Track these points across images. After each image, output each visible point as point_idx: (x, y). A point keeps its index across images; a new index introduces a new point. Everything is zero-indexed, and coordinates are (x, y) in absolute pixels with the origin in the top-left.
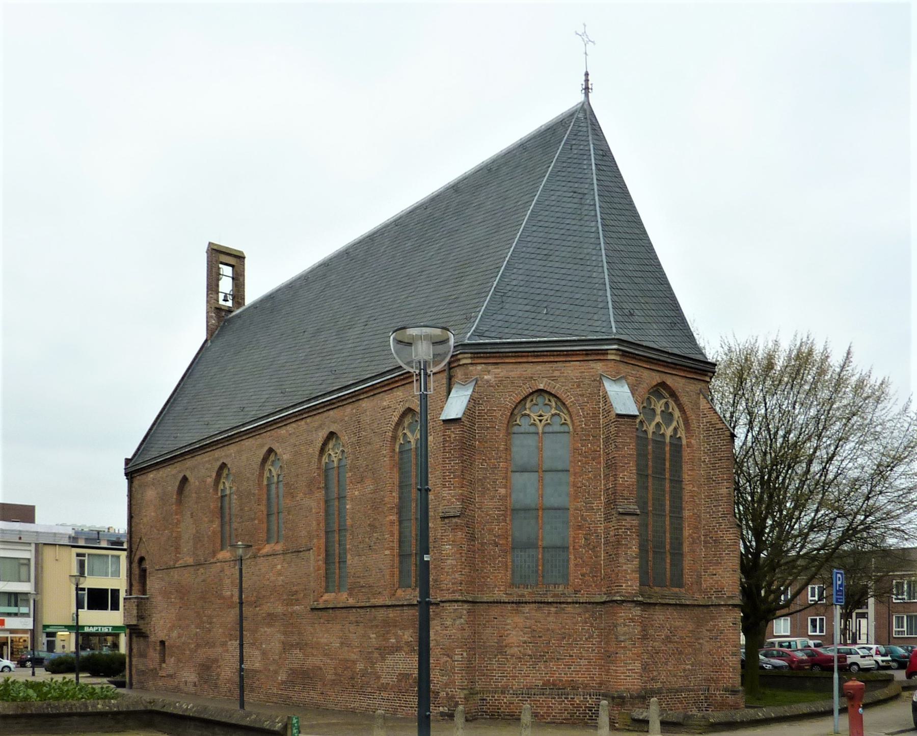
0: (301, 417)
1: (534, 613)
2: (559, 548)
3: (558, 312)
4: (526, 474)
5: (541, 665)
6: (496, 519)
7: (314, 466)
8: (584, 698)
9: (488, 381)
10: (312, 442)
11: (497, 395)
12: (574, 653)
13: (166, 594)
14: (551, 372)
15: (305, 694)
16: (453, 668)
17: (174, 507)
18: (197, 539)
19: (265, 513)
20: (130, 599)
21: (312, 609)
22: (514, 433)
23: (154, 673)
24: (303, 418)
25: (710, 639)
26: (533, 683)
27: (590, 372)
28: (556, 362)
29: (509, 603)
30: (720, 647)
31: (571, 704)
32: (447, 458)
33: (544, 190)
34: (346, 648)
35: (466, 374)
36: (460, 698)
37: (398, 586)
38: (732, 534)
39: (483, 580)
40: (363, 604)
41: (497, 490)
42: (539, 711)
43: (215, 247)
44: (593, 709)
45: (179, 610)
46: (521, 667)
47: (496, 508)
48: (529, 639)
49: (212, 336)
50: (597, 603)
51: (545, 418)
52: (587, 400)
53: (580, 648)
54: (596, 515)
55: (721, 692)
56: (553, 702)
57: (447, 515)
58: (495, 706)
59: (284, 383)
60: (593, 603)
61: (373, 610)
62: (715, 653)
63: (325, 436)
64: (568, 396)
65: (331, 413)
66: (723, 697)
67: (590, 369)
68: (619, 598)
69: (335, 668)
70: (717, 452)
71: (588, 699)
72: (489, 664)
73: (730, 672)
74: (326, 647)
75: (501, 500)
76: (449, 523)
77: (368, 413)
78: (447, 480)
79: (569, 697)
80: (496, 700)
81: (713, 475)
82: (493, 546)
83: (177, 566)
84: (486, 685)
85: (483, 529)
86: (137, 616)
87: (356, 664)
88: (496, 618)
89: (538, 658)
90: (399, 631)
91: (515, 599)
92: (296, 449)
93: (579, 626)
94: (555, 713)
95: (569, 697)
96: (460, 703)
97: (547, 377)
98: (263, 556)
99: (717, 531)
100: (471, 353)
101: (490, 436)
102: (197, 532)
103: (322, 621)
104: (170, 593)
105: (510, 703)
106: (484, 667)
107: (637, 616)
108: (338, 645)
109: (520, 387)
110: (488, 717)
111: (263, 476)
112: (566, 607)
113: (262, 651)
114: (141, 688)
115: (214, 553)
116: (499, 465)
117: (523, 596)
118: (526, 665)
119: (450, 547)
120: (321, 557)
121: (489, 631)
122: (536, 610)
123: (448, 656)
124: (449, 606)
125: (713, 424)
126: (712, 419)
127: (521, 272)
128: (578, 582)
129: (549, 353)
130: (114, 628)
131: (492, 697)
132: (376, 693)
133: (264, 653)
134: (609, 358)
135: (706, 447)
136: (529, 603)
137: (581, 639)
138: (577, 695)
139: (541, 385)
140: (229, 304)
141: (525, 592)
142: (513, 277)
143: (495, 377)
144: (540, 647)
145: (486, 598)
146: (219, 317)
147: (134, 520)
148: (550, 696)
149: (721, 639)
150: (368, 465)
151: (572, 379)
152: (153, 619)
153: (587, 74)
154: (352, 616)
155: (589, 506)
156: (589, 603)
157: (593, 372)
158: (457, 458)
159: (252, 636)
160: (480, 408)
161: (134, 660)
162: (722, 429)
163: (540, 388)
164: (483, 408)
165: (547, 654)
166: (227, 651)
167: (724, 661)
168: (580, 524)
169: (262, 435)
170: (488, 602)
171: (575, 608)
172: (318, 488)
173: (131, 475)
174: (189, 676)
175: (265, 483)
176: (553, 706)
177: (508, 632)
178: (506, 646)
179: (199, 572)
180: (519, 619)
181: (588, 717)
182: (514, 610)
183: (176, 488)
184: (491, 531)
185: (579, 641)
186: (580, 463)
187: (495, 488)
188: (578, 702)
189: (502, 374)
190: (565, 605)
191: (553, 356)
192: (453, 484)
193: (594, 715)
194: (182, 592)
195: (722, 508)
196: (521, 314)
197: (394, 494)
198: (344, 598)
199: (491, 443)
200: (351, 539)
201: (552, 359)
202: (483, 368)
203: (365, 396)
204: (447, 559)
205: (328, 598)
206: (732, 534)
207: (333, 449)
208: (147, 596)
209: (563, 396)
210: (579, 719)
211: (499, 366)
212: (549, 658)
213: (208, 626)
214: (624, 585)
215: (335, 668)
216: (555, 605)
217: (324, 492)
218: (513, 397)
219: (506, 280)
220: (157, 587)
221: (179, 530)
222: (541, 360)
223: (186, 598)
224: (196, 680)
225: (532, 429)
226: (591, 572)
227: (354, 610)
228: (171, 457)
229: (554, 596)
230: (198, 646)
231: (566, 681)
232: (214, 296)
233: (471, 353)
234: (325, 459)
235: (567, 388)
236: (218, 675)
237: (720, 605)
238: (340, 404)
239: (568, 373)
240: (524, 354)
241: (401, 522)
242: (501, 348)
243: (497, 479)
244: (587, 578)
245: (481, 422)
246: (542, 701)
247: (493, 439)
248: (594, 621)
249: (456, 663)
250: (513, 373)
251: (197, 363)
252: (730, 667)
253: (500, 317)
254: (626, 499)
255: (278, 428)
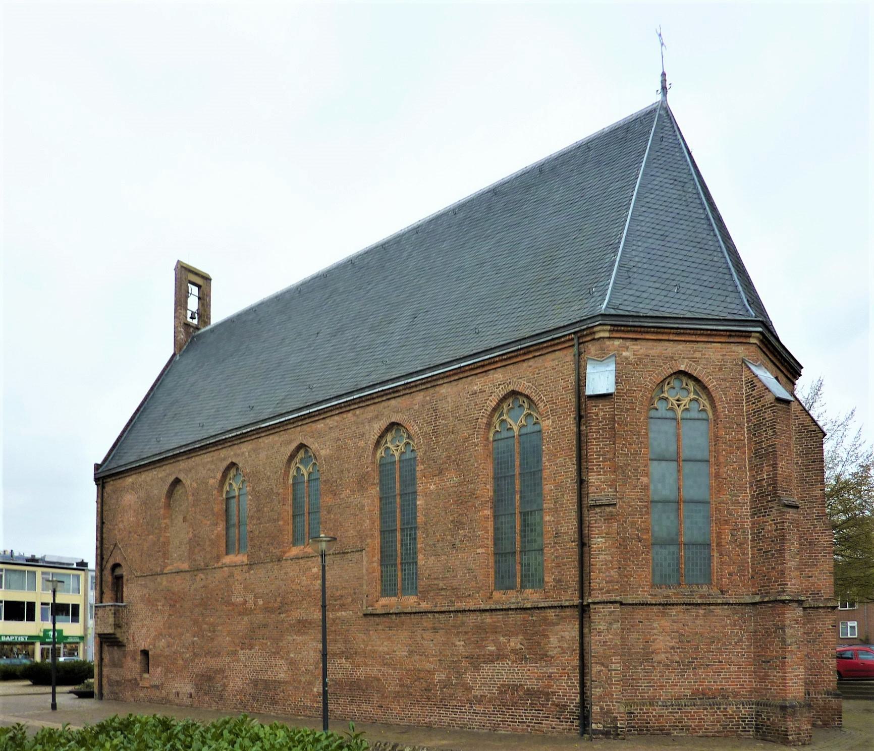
0: (348, 408)
1: (681, 616)
2: (700, 544)
3: (689, 292)
4: (664, 464)
5: (690, 672)
6: (639, 511)
7: (367, 459)
8: (736, 708)
9: (626, 358)
10: (363, 435)
11: (636, 374)
12: (724, 659)
13: (150, 602)
14: (692, 352)
15: (354, 707)
16: (610, 678)
17: (162, 511)
18: (195, 543)
19: (291, 513)
20: (100, 607)
21: (365, 615)
22: (652, 418)
23: (134, 684)
24: (351, 410)
25: (808, 642)
26: (681, 692)
27: (732, 355)
28: (697, 342)
29: (655, 605)
30: (819, 650)
31: (724, 715)
32: (594, 439)
33: (644, 174)
34: (418, 657)
35: (602, 349)
36: (619, 713)
37: (493, 588)
38: (827, 536)
39: (626, 580)
40: (443, 609)
41: (639, 479)
42: (690, 724)
43: (185, 266)
44: (747, 720)
45: (168, 618)
46: (668, 676)
47: (639, 499)
48: (677, 645)
49: (180, 349)
50: (747, 604)
51: (684, 402)
52: (730, 385)
53: (730, 652)
54: (742, 509)
55: (823, 696)
56: (705, 713)
57: (598, 503)
58: (643, 720)
59: (306, 380)
60: (742, 604)
61: (459, 615)
62: (813, 656)
63: (383, 428)
64: (710, 379)
65: (393, 402)
66: (825, 701)
67: (732, 352)
68: (787, 598)
69: (400, 680)
70: (810, 454)
71: (741, 709)
72: (634, 672)
73: (830, 675)
74: (388, 656)
75: (642, 489)
76: (601, 512)
77: (449, 399)
78: (595, 463)
79: (722, 707)
80: (644, 713)
81: (806, 477)
82: (637, 541)
83: (165, 572)
84: (632, 696)
85: (625, 522)
86: (114, 625)
87: (434, 674)
88: (642, 622)
89: (688, 665)
90: (502, 638)
91: (662, 601)
92: (340, 443)
93: (728, 629)
94: (707, 725)
95: (722, 707)
96: (619, 718)
97: (688, 358)
98: (291, 559)
99: (812, 533)
100: (611, 325)
101: (630, 419)
102: (195, 536)
103: (380, 627)
104: (157, 600)
105: (659, 716)
106: (630, 676)
107: (800, 617)
108: (405, 653)
109: (661, 366)
110: (636, 732)
111: (289, 474)
112: (713, 609)
113: (288, 661)
114: (115, 699)
115: (218, 558)
116: (641, 451)
117: (668, 597)
118: (675, 672)
119: (603, 540)
120: (375, 559)
121: (634, 635)
122: (684, 613)
123: (603, 664)
124: (603, 608)
125: (805, 426)
126: (804, 421)
127: (640, 249)
128: (726, 582)
129: (692, 331)
130: (30, 637)
131: (640, 710)
132: (465, 706)
133: (292, 663)
134: (751, 342)
135: (799, 449)
136: (677, 604)
137: (730, 643)
138: (730, 705)
139: (682, 366)
140: (195, 322)
141: (670, 592)
142: (634, 253)
143: (634, 355)
144: (688, 652)
145: (630, 600)
146: (187, 333)
147: (107, 526)
148: (702, 707)
149: (819, 642)
150: (449, 456)
151: (713, 362)
152: (132, 627)
153: (664, 75)
154: (428, 621)
155: (736, 500)
156: (739, 604)
157: (735, 355)
158: (608, 438)
159: (275, 646)
160: (619, 387)
161: (106, 671)
162: (815, 431)
163: (680, 369)
164: (622, 388)
165: (695, 661)
166: (238, 660)
167: (823, 663)
168: (726, 518)
169: (289, 431)
170: (633, 604)
171: (723, 609)
172: (373, 484)
173: (103, 480)
174: (184, 687)
175: (291, 481)
176: (705, 718)
177: (655, 637)
178: (653, 653)
179: (198, 578)
180: (665, 623)
181: (741, 729)
182: (659, 612)
183: (165, 491)
184: (633, 524)
185: (728, 645)
186: (724, 452)
187: (637, 476)
188: (731, 712)
189: (641, 351)
190: (713, 607)
191: (696, 335)
192: (603, 468)
193: (747, 727)
194: (174, 600)
195: (816, 510)
196: (651, 290)
197: (488, 487)
198: (411, 602)
199: (632, 427)
200: (424, 538)
201: (693, 338)
202: (621, 343)
203: (446, 380)
204: (598, 554)
205: (385, 603)
206: (827, 536)
207: (392, 442)
208: (124, 604)
209: (705, 380)
210: (733, 731)
211: (639, 342)
212: (698, 665)
213: (209, 634)
214: (789, 583)
215: (400, 680)
216: (703, 607)
217: (378, 489)
218: (654, 377)
219: (627, 256)
220: (137, 594)
221: (168, 535)
222: (683, 339)
223: (178, 605)
224: (193, 691)
225: (670, 414)
226: (738, 571)
227: (430, 615)
228: (159, 460)
229: (701, 597)
230: (195, 655)
231: (716, 689)
232: (183, 312)
233: (611, 325)
234: (309, 469)
235: (709, 371)
236: (225, 686)
237: (818, 607)
238: (407, 391)
239: (710, 355)
240: (666, 330)
241: (496, 517)
242: (644, 322)
243: (639, 467)
244: (734, 577)
245: (621, 402)
246: (694, 712)
247: (633, 422)
248: (743, 623)
249: (613, 672)
250: (654, 351)
251: (166, 375)
252: (831, 670)
253: (630, 292)
254: (785, 491)
255: (312, 422)
